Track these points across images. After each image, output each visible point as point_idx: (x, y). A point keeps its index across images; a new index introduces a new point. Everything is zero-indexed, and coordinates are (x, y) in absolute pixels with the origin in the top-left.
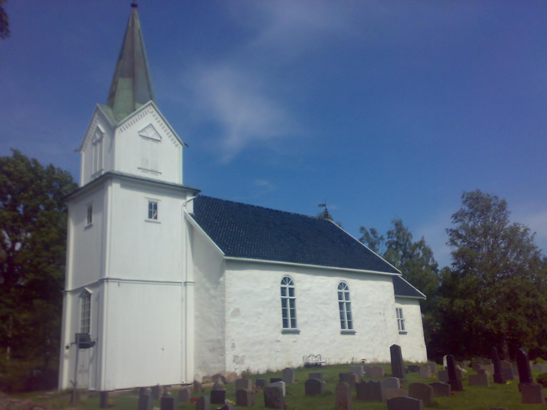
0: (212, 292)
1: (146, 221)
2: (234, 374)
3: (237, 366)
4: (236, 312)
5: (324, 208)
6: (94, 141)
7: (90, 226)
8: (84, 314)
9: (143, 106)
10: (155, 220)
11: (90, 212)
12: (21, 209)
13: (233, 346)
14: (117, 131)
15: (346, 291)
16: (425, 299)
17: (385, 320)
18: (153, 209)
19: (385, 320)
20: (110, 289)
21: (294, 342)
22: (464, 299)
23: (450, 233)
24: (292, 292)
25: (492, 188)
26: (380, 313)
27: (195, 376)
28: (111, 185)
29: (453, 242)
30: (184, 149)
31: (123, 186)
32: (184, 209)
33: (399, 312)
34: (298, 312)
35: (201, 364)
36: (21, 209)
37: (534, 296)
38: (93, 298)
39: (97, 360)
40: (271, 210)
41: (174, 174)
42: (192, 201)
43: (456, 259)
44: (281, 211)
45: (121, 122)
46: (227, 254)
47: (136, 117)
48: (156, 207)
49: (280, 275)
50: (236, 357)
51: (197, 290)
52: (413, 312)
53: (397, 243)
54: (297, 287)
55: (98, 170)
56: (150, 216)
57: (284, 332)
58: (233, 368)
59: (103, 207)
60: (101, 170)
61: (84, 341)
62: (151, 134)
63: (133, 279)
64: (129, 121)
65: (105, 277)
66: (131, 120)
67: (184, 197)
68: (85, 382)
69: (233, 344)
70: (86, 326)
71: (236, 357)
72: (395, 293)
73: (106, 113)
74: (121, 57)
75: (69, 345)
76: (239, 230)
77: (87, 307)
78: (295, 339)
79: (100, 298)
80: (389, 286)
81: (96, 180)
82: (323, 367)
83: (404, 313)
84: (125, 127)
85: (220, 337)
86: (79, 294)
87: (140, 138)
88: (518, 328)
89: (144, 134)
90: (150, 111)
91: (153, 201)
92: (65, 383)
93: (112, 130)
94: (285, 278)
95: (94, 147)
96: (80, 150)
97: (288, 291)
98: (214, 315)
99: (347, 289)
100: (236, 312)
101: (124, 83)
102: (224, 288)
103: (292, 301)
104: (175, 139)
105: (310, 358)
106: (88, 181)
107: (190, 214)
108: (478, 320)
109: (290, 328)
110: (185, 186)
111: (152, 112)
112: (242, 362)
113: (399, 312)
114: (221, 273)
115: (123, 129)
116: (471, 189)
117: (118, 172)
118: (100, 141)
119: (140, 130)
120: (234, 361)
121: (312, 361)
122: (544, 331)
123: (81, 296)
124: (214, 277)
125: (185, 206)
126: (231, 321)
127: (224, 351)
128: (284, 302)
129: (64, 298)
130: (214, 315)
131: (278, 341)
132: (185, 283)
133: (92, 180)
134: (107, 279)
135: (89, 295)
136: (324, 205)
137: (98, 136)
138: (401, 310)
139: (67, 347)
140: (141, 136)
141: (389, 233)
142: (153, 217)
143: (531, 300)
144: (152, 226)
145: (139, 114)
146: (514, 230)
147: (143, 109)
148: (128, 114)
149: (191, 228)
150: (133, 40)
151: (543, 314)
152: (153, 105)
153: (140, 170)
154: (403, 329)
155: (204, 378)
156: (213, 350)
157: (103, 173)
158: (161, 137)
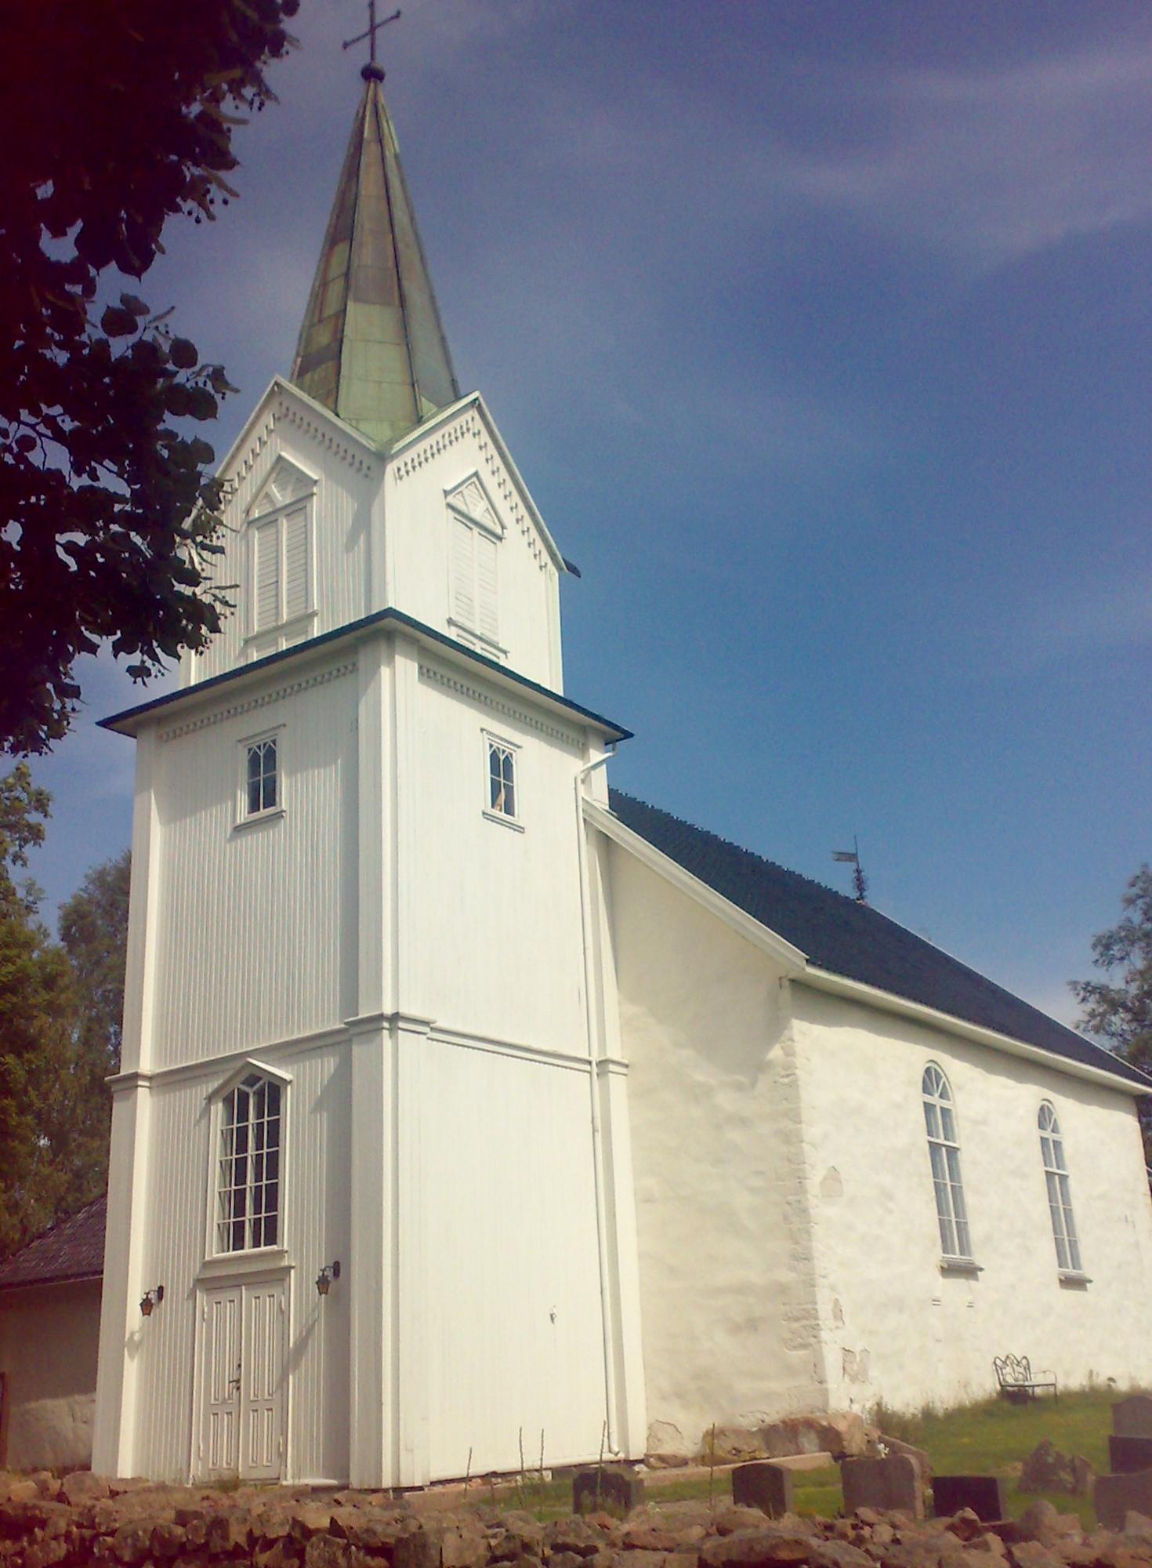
0: (726, 1100)
5: (852, 866)
13: (838, 1314)
15: (1055, 1136)
51: (640, 1094)
58: (848, 1400)
62: (479, 511)
65: (388, 1009)
67: (582, 751)
68: (274, 1454)
82: (1034, 1399)
85: (786, 1276)
102: (794, 1085)
114: (775, 1029)
118: (298, 507)
126: (824, 1212)
131: (936, 1301)
132: (600, 1063)
134: (396, 1017)
136: (852, 857)
140: (450, 506)
158: (503, 528)
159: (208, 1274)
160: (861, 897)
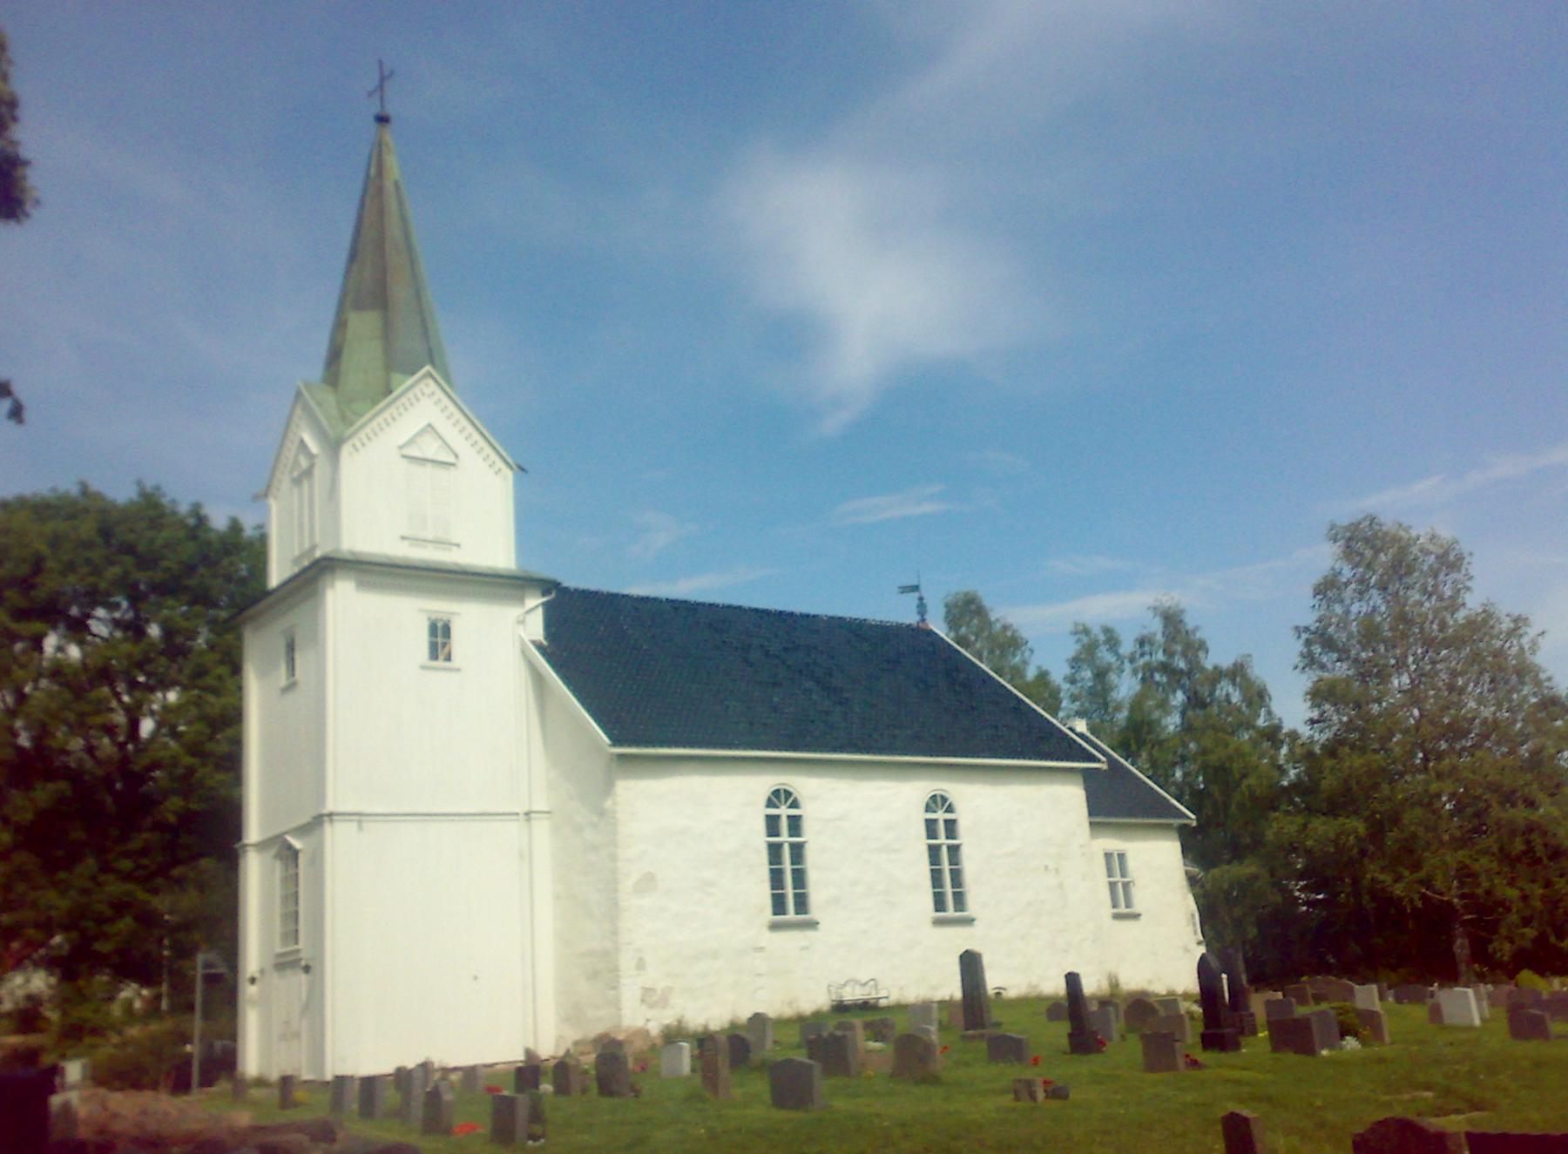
1: (424, 668)
2: (644, 1033)
3: (651, 1013)
4: (648, 882)
5: (916, 595)
6: (296, 474)
7: (291, 687)
8: (285, 899)
9: (410, 381)
10: (447, 664)
11: (291, 648)
12: (154, 631)
13: (641, 965)
14: (346, 450)
16: (1194, 824)
17: (1061, 886)
18: (440, 637)
19: (1061, 886)
20: (337, 837)
21: (804, 948)
22: (1336, 816)
23: (1304, 636)
24: (795, 824)
25: (1417, 507)
26: (1046, 868)
27: (560, 1038)
28: (332, 586)
29: (1310, 661)
30: (515, 475)
31: (362, 585)
32: (520, 631)
33: (1115, 863)
34: (813, 876)
35: (572, 1013)
36: (154, 631)
37: (1531, 804)
38: (302, 860)
39: (314, 1007)
40: (767, 613)
41: (495, 549)
42: (540, 611)
43: (1315, 705)
44: (792, 614)
45: (359, 423)
46: (617, 741)
47: (392, 410)
48: (447, 631)
49: (760, 784)
50: (647, 991)
52: (1159, 861)
53: (1165, 668)
54: (809, 812)
55: (307, 545)
56: (434, 655)
57: (774, 927)
58: (638, 1017)
59: (316, 637)
60: (313, 548)
61: (286, 963)
62: (430, 448)
63: (394, 810)
64: (374, 424)
65: (325, 811)
66: (380, 419)
67: (521, 600)
69: (641, 960)
70: (292, 927)
71: (647, 991)
72: (1090, 814)
73: (319, 404)
74: (353, 257)
75: (257, 975)
76: (656, 674)
77: (291, 880)
78: (803, 943)
79: (317, 858)
80: (1072, 796)
81: (304, 571)
83: (1132, 864)
84: (365, 439)
86: (273, 851)
87: (405, 461)
88: (1479, 891)
89: (414, 451)
90: (427, 391)
91: (439, 616)
92: (252, 1062)
93: (334, 447)
94: (776, 793)
95: (296, 490)
96: (266, 495)
97: (784, 824)
98: (596, 891)
99: (950, 809)
100: (648, 882)
101: (364, 324)
103: (798, 851)
104: (494, 457)
105: (848, 989)
106: (287, 574)
107: (534, 642)
108: (1374, 872)
109: (951, 912)
110: (520, 574)
111: (433, 393)
112: (664, 1002)
113: (1115, 863)
114: (608, 789)
115: (358, 444)
116: (1347, 511)
117: (353, 553)
118: (308, 473)
119: (401, 442)
120: (643, 1001)
121: (851, 994)
122: (1553, 903)
123: (278, 856)
124: (598, 795)
125: (521, 622)
127: (618, 977)
128: (774, 851)
129: (242, 863)
130: (596, 891)
131: (761, 949)
132: (527, 814)
133: (296, 570)
134: (330, 815)
135: (295, 854)
136: (916, 588)
137: (304, 463)
138: (1121, 856)
139: (253, 981)
141: (1142, 642)
142: (441, 657)
143: (1520, 814)
144: (440, 680)
145: (398, 403)
146: (1481, 625)
147: (412, 386)
148: (375, 403)
149: (538, 679)
150: (381, 212)
151: (1556, 854)
152: (432, 376)
153: (406, 543)
154: (1127, 906)
155: (576, 1043)
156: (594, 976)
157: (318, 554)
159: (282, 960)
160: (923, 620)
